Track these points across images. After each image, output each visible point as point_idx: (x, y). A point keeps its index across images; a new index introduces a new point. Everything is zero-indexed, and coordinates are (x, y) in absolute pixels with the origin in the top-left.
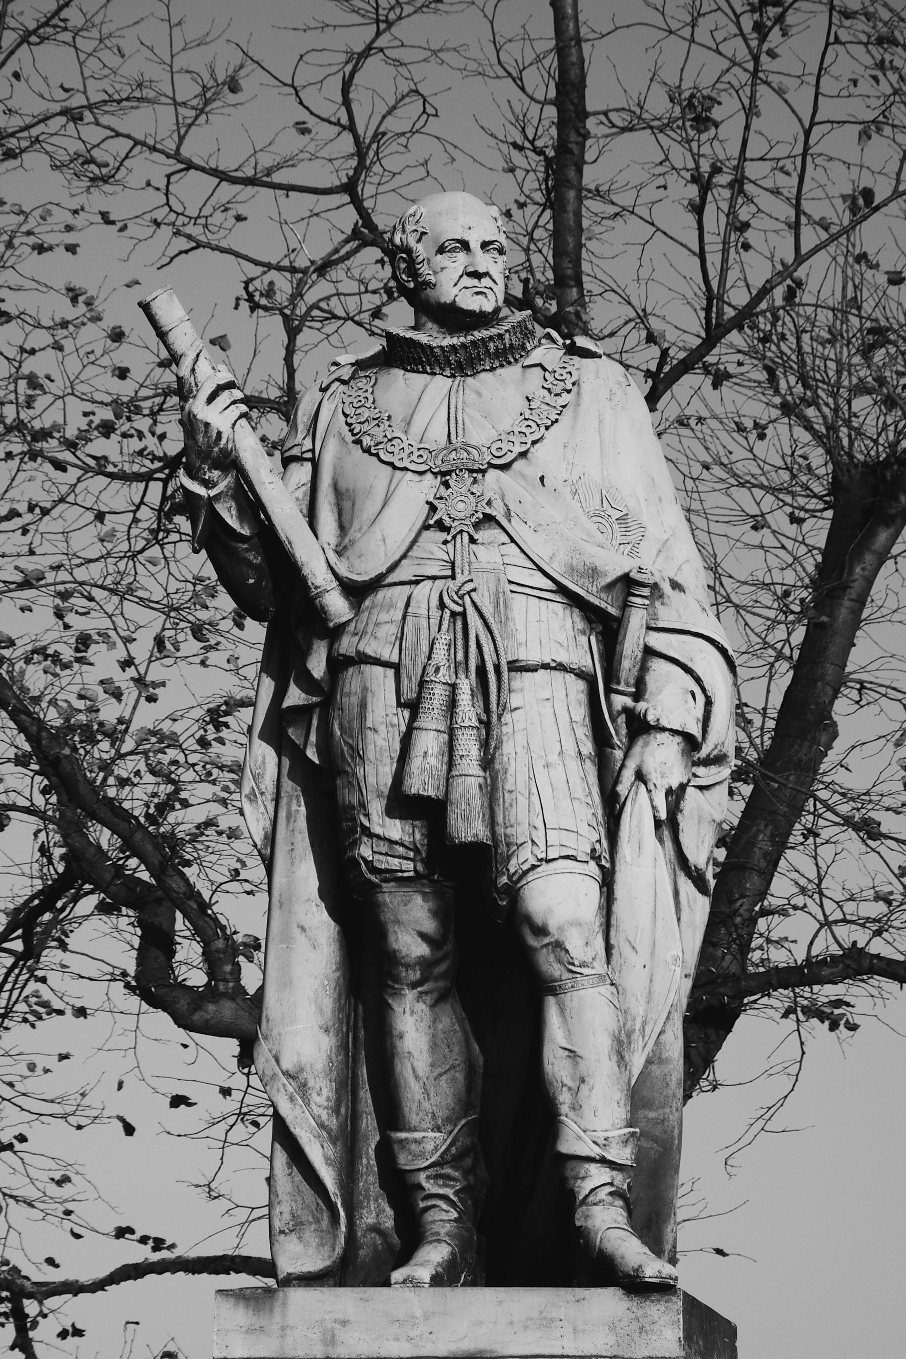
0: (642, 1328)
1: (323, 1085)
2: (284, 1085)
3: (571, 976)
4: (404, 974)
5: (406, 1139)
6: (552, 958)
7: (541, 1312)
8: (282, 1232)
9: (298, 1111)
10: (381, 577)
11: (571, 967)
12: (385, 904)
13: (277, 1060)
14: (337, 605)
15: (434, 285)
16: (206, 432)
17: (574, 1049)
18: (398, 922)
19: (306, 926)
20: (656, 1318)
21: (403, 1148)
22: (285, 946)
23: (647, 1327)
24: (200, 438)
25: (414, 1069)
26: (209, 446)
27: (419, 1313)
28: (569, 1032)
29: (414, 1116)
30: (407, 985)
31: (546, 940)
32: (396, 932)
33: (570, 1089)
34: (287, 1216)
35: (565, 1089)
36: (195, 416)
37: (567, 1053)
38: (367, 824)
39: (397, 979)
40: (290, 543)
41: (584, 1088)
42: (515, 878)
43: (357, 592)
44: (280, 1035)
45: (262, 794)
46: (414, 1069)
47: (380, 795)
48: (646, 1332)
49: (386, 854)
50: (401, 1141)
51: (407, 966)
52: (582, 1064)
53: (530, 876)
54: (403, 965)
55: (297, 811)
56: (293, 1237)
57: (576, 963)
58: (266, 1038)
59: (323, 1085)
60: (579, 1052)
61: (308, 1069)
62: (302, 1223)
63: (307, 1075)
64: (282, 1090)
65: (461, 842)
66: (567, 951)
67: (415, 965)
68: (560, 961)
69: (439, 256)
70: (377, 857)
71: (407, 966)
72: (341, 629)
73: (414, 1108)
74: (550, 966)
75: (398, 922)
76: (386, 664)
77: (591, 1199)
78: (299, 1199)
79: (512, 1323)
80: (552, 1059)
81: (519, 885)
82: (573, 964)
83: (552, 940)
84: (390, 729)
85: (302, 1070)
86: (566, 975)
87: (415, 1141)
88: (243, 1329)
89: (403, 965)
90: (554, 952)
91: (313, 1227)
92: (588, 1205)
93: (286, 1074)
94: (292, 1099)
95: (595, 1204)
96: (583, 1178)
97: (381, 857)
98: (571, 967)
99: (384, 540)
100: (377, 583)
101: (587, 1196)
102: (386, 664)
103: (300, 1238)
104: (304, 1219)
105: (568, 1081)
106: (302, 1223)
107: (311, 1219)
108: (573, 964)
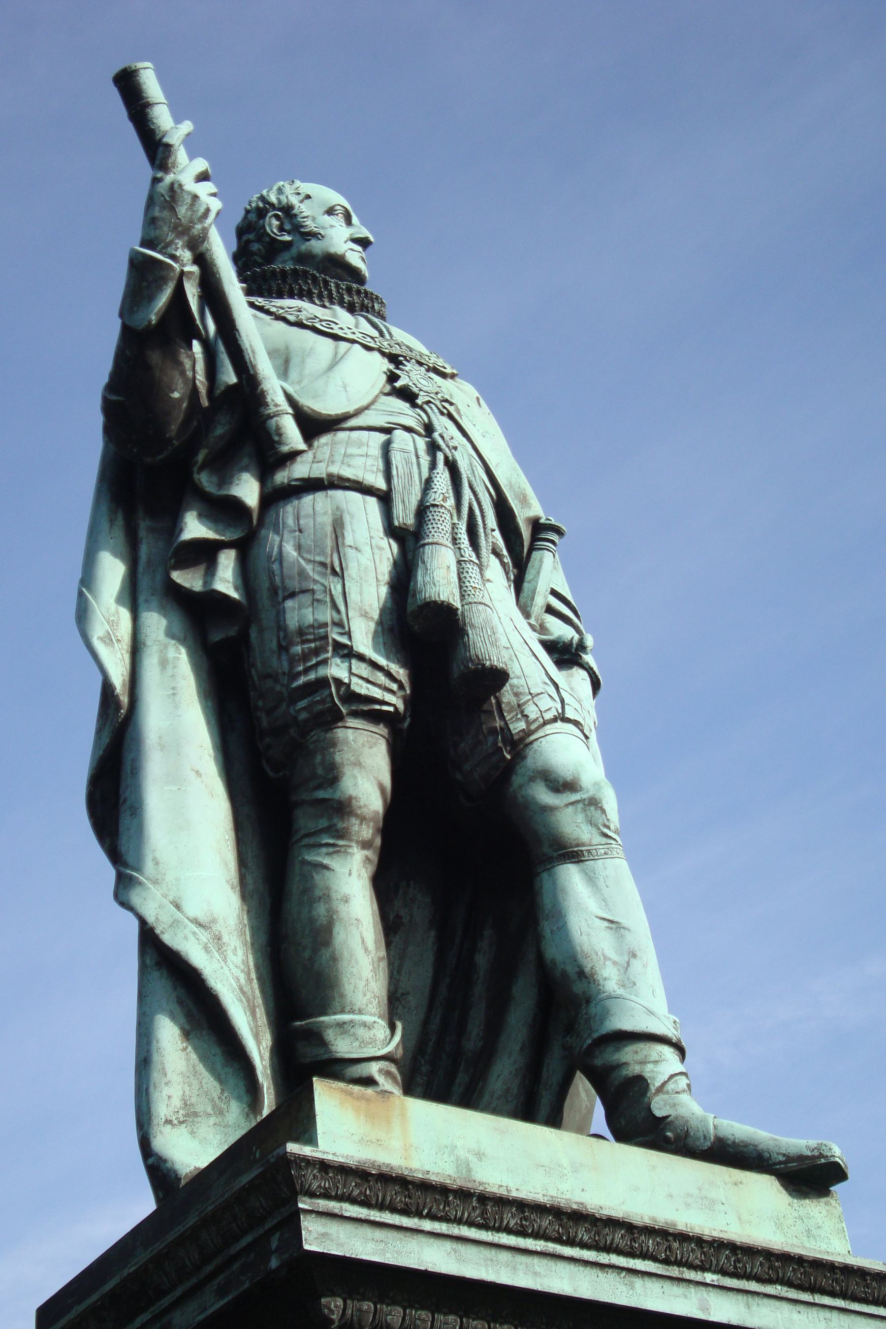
0: (809, 1231)
1: (237, 945)
2: (194, 933)
3: (604, 840)
4: (356, 828)
5: (352, 1021)
6: (580, 818)
7: (700, 1189)
8: (168, 1122)
9: (216, 966)
10: (347, 417)
11: (606, 830)
12: (346, 742)
13: (178, 907)
14: (292, 434)
16: (192, 205)
17: (616, 920)
18: (358, 764)
19: (202, 771)
20: (820, 1221)
21: (345, 1032)
22: (175, 788)
23: (814, 1232)
25: (363, 941)
26: (191, 222)
27: (565, 1162)
28: (605, 902)
29: (359, 996)
30: (357, 842)
32: (355, 777)
33: (615, 963)
34: (177, 1102)
35: (608, 963)
36: (181, 186)
37: (606, 924)
38: (344, 640)
39: (342, 834)
40: (253, 352)
42: (533, 727)
43: (314, 426)
44: (178, 880)
45: (118, 641)
46: (363, 941)
47: (365, 615)
48: (814, 1237)
50: (341, 1025)
51: (363, 819)
52: (629, 937)
53: (549, 729)
54: (357, 816)
55: (178, 659)
56: (183, 1130)
57: (612, 827)
58: (156, 882)
59: (237, 945)
60: (624, 922)
61: (221, 922)
62: (196, 1114)
63: (218, 927)
65: (492, 666)
66: (604, 811)
67: (372, 819)
68: (591, 822)
69: (326, 217)
70: (355, 680)
71: (363, 819)
72: (294, 455)
73: (361, 985)
74: (573, 825)
75: (358, 764)
76: (366, 490)
78: (195, 1083)
79: (671, 1196)
80: (585, 928)
81: (532, 738)
82: (608, 827)
85: (214, 921)
87: (364, 1025)
88: (356, 1138)
89: (357, 816)
90: (584, 810)
91: (212, 1120)
94: (206, 949)
96: (656, 1062)
99: (345, 387)
101: (665, 1083)
102: (366, 490)
104: (199, 1109)
106: (196, 1114)
107: (209, 1110)
108: (608, 827)
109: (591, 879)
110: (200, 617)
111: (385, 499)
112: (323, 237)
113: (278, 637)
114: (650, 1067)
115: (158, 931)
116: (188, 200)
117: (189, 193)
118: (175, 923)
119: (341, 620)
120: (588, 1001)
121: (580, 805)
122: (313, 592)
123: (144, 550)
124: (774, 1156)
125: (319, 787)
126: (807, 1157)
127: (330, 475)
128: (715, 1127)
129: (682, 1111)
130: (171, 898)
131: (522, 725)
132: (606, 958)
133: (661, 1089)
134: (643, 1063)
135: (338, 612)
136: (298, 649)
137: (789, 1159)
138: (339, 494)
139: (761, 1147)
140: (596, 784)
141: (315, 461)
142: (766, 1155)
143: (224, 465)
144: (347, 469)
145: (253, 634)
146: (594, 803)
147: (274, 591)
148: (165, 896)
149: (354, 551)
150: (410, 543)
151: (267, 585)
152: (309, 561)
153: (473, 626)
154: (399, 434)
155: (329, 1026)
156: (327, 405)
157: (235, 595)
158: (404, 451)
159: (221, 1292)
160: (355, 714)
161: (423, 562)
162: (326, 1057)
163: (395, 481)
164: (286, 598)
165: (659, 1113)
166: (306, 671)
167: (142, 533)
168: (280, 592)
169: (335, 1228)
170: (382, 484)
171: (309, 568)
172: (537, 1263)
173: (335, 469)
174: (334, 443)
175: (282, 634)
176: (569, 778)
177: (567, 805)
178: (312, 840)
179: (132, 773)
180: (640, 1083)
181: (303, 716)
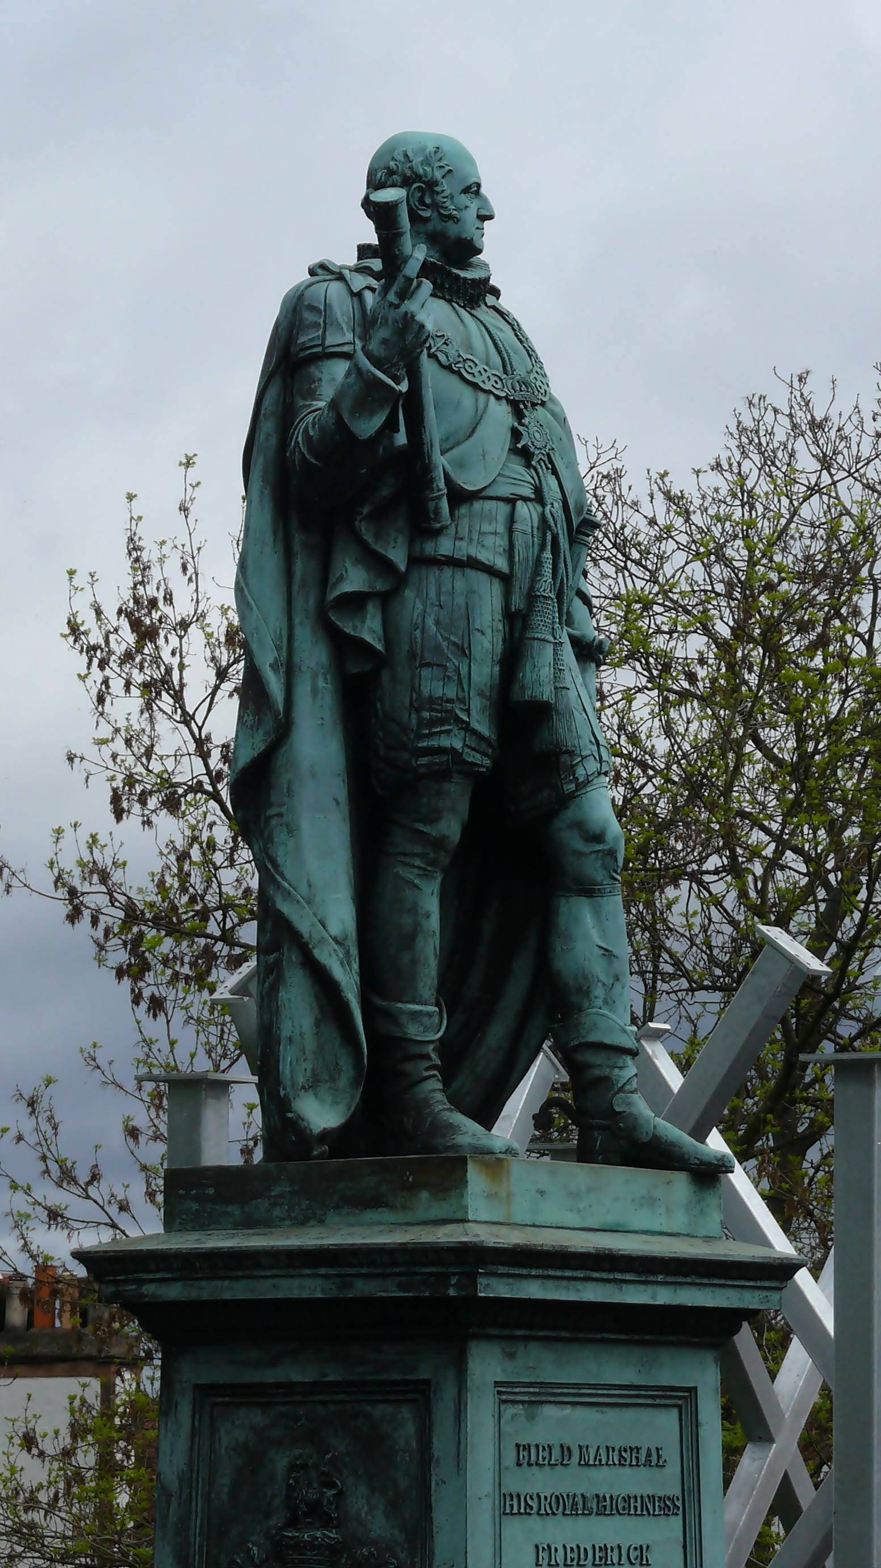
2: (335, 950)
5: (421, 1011)
6: (599, 863)
8: (303, 1087)
11: (614, 874)
15: (458, 220)
17: (610, 948)
24: (410, 338)
31: (600, 847)
33: (604, 984)
37: (602, 952)
41: (618, 986)
44: (324, 901)
49: (473, 749)
64: (334, 955)
68: (605, 867)
70: (466, 750)
77: (627, 1087)
83: (606, 847)
84: (495, 633)
86: (607, 881)
91: (328, 1085)
92: (624, 1092)
93: (335, 939)
95: (632, 1092)
96: (621, 1068)
97: (469, 751)
98: (614, 874)
100: (476, 495)
103: (316, 1094)
105: (603, 978)
107: (327, 1078)
108: (616, 872)
109: (597, 912)
110: (343, 647)
111: (506, 580)
112: (458, 220)
113: (411, 697)
114: (616, 1071)
115: (310, 946)
116: (416, 328)
117: (418, 322)
118: (322, 941)
119: (464, 698)
120: (580, 1010)
121: (600, 854)
122: (445, 667)
123: (298, 567)
124: (692, 1158)
125: (420, 821)
126: (714, 1164)
127: (469, 557)
128: (655, 1127)
129: (634, 1110)
130: (319, 917)
131: (572, 787)
132: (599, 981)
133: (621, 1090)
134: (613, 1067)
135: (463, 690)
136: (426, 714)
137: (702, 1163)
138: (472, 574)
139: (684, 1150)
140: (616, 839)
141: (458, 538)
142: (687, 1156)
143: (380, 516)
144: (483, 551)
145: (385, 676)
146: (612, 853)
147: (412, 655)
148: (315, 915)
149: (479, 634)
150: (519, 624)
151: (407, 647)
152: (445, 639)
153: (558, 713)
154: (519, 504)
155: (403, 1012)
156: (470, 482)
157: (379, 647)
158: (524, 533)
159: (402, 1287)
160: (459, 772)
161: (532, 657)
162: (399, 1035)
163: (516, 567)
164: (422, 666)
165: (618, 1109)
166: (431, 735)
167: (297, 547)
168: (418, 659)
169: (493, 1282)
170: (501, 563)
171: (444, 644)
172: (579, 1285)
173: (473, 551)
174: (471, 515)
175: (414, 696)
176: (598, 832)
177: (591, 853)
178: (407, 860)
179: (289, 790)
180: (607, 1081)
181: (422, 770)
